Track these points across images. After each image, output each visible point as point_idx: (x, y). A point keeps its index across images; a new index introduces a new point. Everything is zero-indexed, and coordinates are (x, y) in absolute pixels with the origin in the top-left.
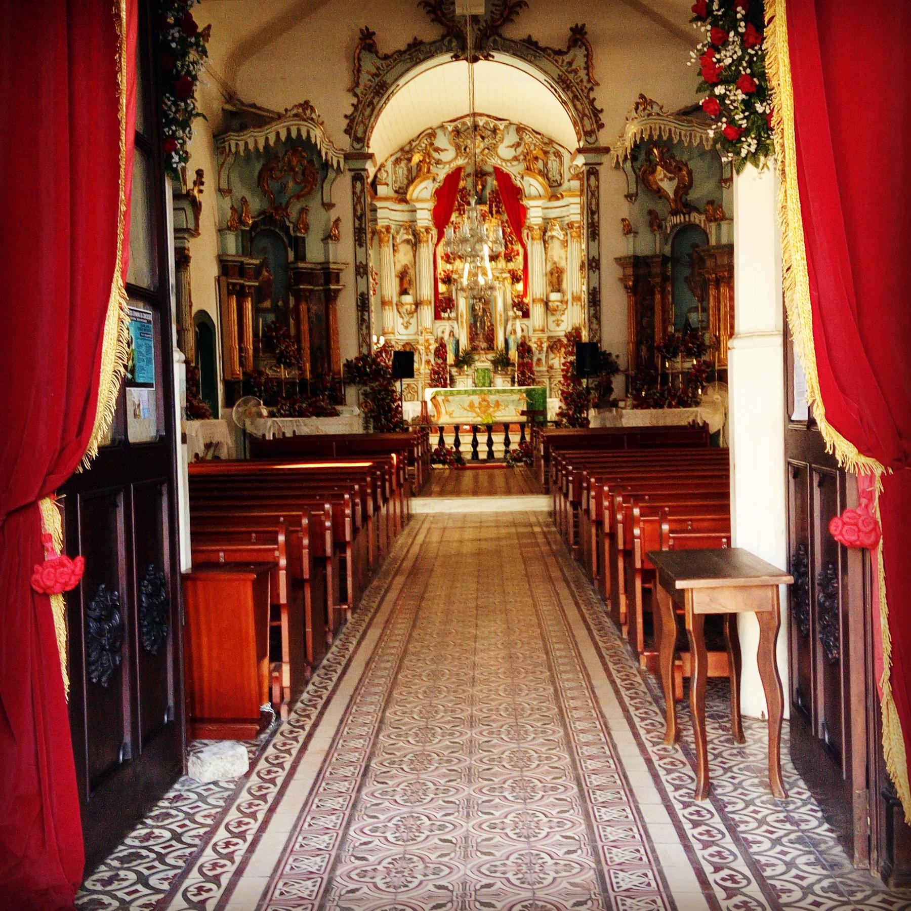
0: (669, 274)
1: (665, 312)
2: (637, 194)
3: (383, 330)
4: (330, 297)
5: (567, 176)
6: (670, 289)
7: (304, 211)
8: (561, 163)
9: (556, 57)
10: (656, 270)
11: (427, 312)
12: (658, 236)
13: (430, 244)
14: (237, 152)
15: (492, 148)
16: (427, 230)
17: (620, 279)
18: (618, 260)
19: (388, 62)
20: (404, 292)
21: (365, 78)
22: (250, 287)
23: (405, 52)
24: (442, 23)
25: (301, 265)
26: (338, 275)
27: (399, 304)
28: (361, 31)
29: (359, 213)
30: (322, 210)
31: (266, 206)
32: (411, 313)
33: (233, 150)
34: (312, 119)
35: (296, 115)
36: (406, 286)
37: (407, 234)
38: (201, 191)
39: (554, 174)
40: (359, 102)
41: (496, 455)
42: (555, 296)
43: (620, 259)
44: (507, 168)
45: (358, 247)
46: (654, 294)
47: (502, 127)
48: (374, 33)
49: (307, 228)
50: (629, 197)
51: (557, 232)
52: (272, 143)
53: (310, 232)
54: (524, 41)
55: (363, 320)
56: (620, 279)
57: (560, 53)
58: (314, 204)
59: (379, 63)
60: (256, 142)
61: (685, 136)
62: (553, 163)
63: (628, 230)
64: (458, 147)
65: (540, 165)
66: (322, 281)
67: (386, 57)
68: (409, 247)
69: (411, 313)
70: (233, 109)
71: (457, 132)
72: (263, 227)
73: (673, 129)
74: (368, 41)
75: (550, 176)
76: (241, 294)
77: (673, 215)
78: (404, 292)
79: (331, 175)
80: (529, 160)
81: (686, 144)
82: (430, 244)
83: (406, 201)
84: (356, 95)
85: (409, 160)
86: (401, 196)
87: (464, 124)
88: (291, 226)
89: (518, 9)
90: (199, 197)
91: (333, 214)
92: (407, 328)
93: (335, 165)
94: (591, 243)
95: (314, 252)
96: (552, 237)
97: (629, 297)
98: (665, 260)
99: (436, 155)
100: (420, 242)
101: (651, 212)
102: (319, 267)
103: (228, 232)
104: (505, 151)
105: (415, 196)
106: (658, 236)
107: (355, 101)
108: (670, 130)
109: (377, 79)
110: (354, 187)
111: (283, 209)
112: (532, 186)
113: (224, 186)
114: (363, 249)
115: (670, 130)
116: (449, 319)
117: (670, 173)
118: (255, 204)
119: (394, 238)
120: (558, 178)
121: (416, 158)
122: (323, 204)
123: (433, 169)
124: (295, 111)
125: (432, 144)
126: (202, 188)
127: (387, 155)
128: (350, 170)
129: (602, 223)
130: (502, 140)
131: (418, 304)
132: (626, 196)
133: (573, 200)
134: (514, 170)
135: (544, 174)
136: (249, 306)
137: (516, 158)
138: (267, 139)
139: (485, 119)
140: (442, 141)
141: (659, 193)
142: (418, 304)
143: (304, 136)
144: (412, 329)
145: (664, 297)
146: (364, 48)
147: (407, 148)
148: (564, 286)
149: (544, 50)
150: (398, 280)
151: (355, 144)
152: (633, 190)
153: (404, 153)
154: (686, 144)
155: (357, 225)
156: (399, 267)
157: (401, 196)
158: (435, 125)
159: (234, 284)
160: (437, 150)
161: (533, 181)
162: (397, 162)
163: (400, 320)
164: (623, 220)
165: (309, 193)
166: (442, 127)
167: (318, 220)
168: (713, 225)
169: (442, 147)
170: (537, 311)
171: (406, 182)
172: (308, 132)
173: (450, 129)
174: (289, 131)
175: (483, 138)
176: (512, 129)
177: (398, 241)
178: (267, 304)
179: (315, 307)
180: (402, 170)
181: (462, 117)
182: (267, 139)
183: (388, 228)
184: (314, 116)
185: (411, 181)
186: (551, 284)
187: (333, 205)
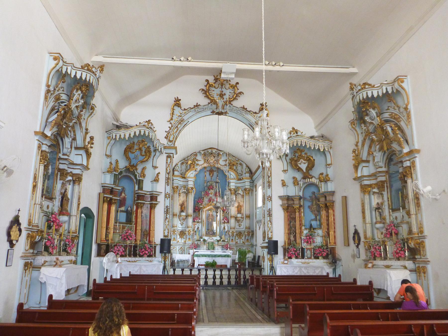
0: (302, 204)
1: (300, 221)
2: (287, 170)
3: (173, 225)
4: (152, 207)
5: (244, 172)
6: (302, 210)
7: (144, 169)
8: (242, 168)
9: (254, 114)
10: (296, 202)
11: (190, 220)
12: (297, 188)
13: (193, 194)
14: (115, 139)
15: (218, 161)
16: (192, 188)
17: (281, 205)
18: (280, 197)
19: (185, 111)
20: (182, 211)
21: (175, 117)
22: (115, 200)
23: (192, 108)
24: (208, 98)
25: (140, 192)
26: (157, 197)
27: (180, 216)
28: (175, 98)
29: (168, 172)
30: (152, 168)
31: (127, 164)
32: (184, 219)
33: (114, 137)
34: (151, 128)
35: (144, 126)
36: (183, 209)
37: (185, 189)
38: (92, 147)
39: (239, 171)
40: (172, 126)
41: (224, 284)
42: (239, 215)
43: (281, 196)
44: (222, 168)
45: (167, 186)
46: (296, 212)
47: (221, 154)
48: (180, 100)
49: (144, 176)
50: (284, 171)
51: (240, 192)
52: (132, 136)
53: (146, 177)
54: (241, 107)
55: (166, 218)
56: (281, 205)
57: (256, 113)
58: (149, 165)
59: (181, 111)
60: (125, 135)
61: (312, 145)
62: (239, 168)
63: (284, 184)
64: (205, 160)
65: (235, 168)
66: (149, 199)
67: (185, 110)
68: (185, 195)
69: (184, 219)
70: (118, 124)
71: (205, 154)
72: (125, 174)
73: (307, 142)
74: (177, 102)
75: (238, 171)
76: (110, 203)
77: (238, 207)
78: (182, 211)
79: (158, 153)
80: (231, 165)
81: (312, 149)
82: (193, 194)
83: (184, 178)
84: (171, 123)
85: (187, 163)
86: (183, 176)
87: (208, 152)
88: (138, 174)
89: (239, 95)
90: (91, 150)
91: (157, 171)
92: (182, 225)
93: (160, 150)
94: (268, 189)
95: (147, 187)
96: (239, 193)
97: (285, 213)
98: (300, 198)
99: (196, 162)
100: (189, 193)
101: (294, 178)
102: (148, 193)
103: (107, 173)
104: (222, 162)
105: (188, 176)
106: (297, 188)
107: (170, 126)
108: (305, 142)
109: (180, 118)
110: (167, 160)
111: (134, 166)
112: (232, 175)
113: (108, 153)
114: (166, 205)
115: (305, 142)
116: (198, 222)
117: (304, 160)
118: (123, 164)
119: (179, 191)
120: (241, 173)
121: (190, 162)
122: (153, 166)
123: (196, 167)
124: (144, 124)
125: (195, 158)
126: (92, 146)
127: (179, 161)
128: (166, 153)
129: (273, 180)
130: (221, 158)
131: (187, 216)
132: (283, 171)
133: (246, 180)
134: (225, 169)
135: (236, 171)
136: (113, 208)
137: (226, 165)
138: (130, 134)
139: (215, 150)
140: (199, 157)
141: (299, 169)
142: (187, 216)
143: (147, 134)
144: (184, 226)
145: (300, 214)
146: (175, 105)
147: (186, 159)
148: (242, 212)
149: (249, 111)
150: (180, 206)
151: (169, 143)
152: (286, 169)
153: (184, 161)
154: (312, 149)
155: (167, 177)
156: (181, 202)
157: (183, 176)
158: (197, 151)
159: (107, 197)
160: (197, 160)
161: (232, 173)
162: (182, 163)
163: (180, 222)
164: (282, 180)
165: (147, 160)
166: (199, 152)
167: (150, 174)
168: (323, 184)
169: (199, 159)
170: (232, 221)
171: (185, 171)
172: (149, 133)
173: (202, 153)
174: (140, 131)
175: (214, 157)
176: (225, 155)
177: (181, 192)
178: (123, 209)
179: (145, 211)
180: (184, 167)
181: (207, 149)
182: (130, 134)
183: (177, 187)
184: (152, 127)
185: (187, 171)
186: (238, 211)
187: (157, 167)
